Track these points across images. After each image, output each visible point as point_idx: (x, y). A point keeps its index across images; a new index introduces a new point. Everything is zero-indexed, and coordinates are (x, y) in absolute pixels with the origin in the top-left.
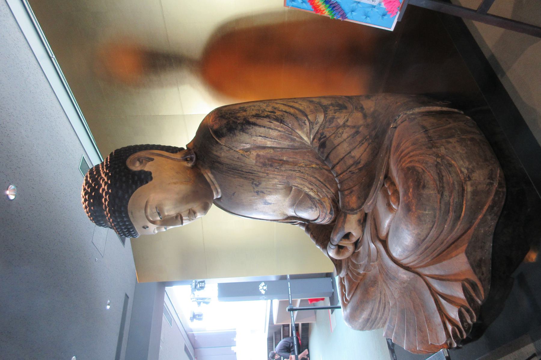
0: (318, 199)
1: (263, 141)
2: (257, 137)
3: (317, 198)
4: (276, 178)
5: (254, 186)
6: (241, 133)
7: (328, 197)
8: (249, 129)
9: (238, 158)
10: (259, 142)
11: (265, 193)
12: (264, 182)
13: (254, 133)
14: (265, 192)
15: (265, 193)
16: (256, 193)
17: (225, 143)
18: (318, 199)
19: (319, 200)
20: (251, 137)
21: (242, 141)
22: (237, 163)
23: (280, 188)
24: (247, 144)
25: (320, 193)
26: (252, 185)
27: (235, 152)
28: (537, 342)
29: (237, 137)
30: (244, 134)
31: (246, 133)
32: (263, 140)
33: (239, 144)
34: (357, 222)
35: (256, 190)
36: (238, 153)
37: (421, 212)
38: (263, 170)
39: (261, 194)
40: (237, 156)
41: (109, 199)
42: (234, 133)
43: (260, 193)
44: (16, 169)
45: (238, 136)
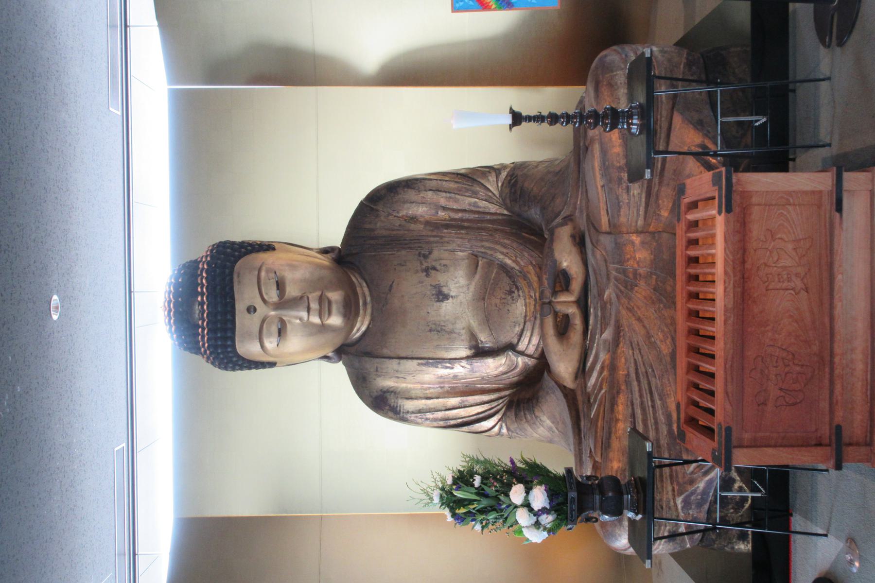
0: (518, 270)
1: (435, 198)
2: (427, 191)
3: (516, 268)
4: (453, 241)
5: (422, 258)
6: (406, 189)
7: (531, 263)
8: (417, 183)
9: (400, 225)
10: (429, 199)
11: (437, 270)
12: (437, 248)
13: (422, 188)
14: (438, 267)
15: (437, 270)
16: (425, 273)
17: (383, 208)
18: (518, 270)
19: (520, 272)
20: (418, 193)
21: (406, 200)
22: (398, 232)
23: (460, 258)
24: (413, 202)
25: (519, 258)
26: (419, 258)
27: (396, 218)
28: (790, 170)
29: (400, 196)
30: (410, 190)
31: (412, 188)
32: (435, 197)
33: (402, 205)
34: (570, 239)
35: (425, 265)
36: (399, 220)
37: (608, 75)
38: (435, 233)
39: (433, 272)
40: (398, 224)
41: (207, 301)
42: (397, 191)
43: (431, 271)
44: (59, 332)
45: (401, 194)
